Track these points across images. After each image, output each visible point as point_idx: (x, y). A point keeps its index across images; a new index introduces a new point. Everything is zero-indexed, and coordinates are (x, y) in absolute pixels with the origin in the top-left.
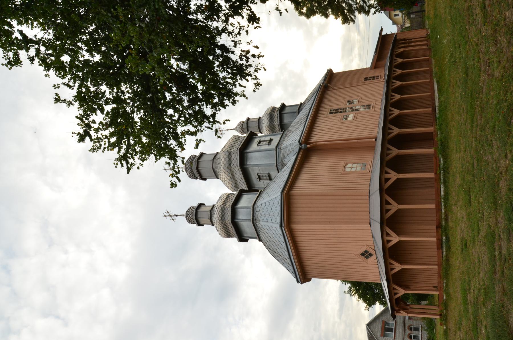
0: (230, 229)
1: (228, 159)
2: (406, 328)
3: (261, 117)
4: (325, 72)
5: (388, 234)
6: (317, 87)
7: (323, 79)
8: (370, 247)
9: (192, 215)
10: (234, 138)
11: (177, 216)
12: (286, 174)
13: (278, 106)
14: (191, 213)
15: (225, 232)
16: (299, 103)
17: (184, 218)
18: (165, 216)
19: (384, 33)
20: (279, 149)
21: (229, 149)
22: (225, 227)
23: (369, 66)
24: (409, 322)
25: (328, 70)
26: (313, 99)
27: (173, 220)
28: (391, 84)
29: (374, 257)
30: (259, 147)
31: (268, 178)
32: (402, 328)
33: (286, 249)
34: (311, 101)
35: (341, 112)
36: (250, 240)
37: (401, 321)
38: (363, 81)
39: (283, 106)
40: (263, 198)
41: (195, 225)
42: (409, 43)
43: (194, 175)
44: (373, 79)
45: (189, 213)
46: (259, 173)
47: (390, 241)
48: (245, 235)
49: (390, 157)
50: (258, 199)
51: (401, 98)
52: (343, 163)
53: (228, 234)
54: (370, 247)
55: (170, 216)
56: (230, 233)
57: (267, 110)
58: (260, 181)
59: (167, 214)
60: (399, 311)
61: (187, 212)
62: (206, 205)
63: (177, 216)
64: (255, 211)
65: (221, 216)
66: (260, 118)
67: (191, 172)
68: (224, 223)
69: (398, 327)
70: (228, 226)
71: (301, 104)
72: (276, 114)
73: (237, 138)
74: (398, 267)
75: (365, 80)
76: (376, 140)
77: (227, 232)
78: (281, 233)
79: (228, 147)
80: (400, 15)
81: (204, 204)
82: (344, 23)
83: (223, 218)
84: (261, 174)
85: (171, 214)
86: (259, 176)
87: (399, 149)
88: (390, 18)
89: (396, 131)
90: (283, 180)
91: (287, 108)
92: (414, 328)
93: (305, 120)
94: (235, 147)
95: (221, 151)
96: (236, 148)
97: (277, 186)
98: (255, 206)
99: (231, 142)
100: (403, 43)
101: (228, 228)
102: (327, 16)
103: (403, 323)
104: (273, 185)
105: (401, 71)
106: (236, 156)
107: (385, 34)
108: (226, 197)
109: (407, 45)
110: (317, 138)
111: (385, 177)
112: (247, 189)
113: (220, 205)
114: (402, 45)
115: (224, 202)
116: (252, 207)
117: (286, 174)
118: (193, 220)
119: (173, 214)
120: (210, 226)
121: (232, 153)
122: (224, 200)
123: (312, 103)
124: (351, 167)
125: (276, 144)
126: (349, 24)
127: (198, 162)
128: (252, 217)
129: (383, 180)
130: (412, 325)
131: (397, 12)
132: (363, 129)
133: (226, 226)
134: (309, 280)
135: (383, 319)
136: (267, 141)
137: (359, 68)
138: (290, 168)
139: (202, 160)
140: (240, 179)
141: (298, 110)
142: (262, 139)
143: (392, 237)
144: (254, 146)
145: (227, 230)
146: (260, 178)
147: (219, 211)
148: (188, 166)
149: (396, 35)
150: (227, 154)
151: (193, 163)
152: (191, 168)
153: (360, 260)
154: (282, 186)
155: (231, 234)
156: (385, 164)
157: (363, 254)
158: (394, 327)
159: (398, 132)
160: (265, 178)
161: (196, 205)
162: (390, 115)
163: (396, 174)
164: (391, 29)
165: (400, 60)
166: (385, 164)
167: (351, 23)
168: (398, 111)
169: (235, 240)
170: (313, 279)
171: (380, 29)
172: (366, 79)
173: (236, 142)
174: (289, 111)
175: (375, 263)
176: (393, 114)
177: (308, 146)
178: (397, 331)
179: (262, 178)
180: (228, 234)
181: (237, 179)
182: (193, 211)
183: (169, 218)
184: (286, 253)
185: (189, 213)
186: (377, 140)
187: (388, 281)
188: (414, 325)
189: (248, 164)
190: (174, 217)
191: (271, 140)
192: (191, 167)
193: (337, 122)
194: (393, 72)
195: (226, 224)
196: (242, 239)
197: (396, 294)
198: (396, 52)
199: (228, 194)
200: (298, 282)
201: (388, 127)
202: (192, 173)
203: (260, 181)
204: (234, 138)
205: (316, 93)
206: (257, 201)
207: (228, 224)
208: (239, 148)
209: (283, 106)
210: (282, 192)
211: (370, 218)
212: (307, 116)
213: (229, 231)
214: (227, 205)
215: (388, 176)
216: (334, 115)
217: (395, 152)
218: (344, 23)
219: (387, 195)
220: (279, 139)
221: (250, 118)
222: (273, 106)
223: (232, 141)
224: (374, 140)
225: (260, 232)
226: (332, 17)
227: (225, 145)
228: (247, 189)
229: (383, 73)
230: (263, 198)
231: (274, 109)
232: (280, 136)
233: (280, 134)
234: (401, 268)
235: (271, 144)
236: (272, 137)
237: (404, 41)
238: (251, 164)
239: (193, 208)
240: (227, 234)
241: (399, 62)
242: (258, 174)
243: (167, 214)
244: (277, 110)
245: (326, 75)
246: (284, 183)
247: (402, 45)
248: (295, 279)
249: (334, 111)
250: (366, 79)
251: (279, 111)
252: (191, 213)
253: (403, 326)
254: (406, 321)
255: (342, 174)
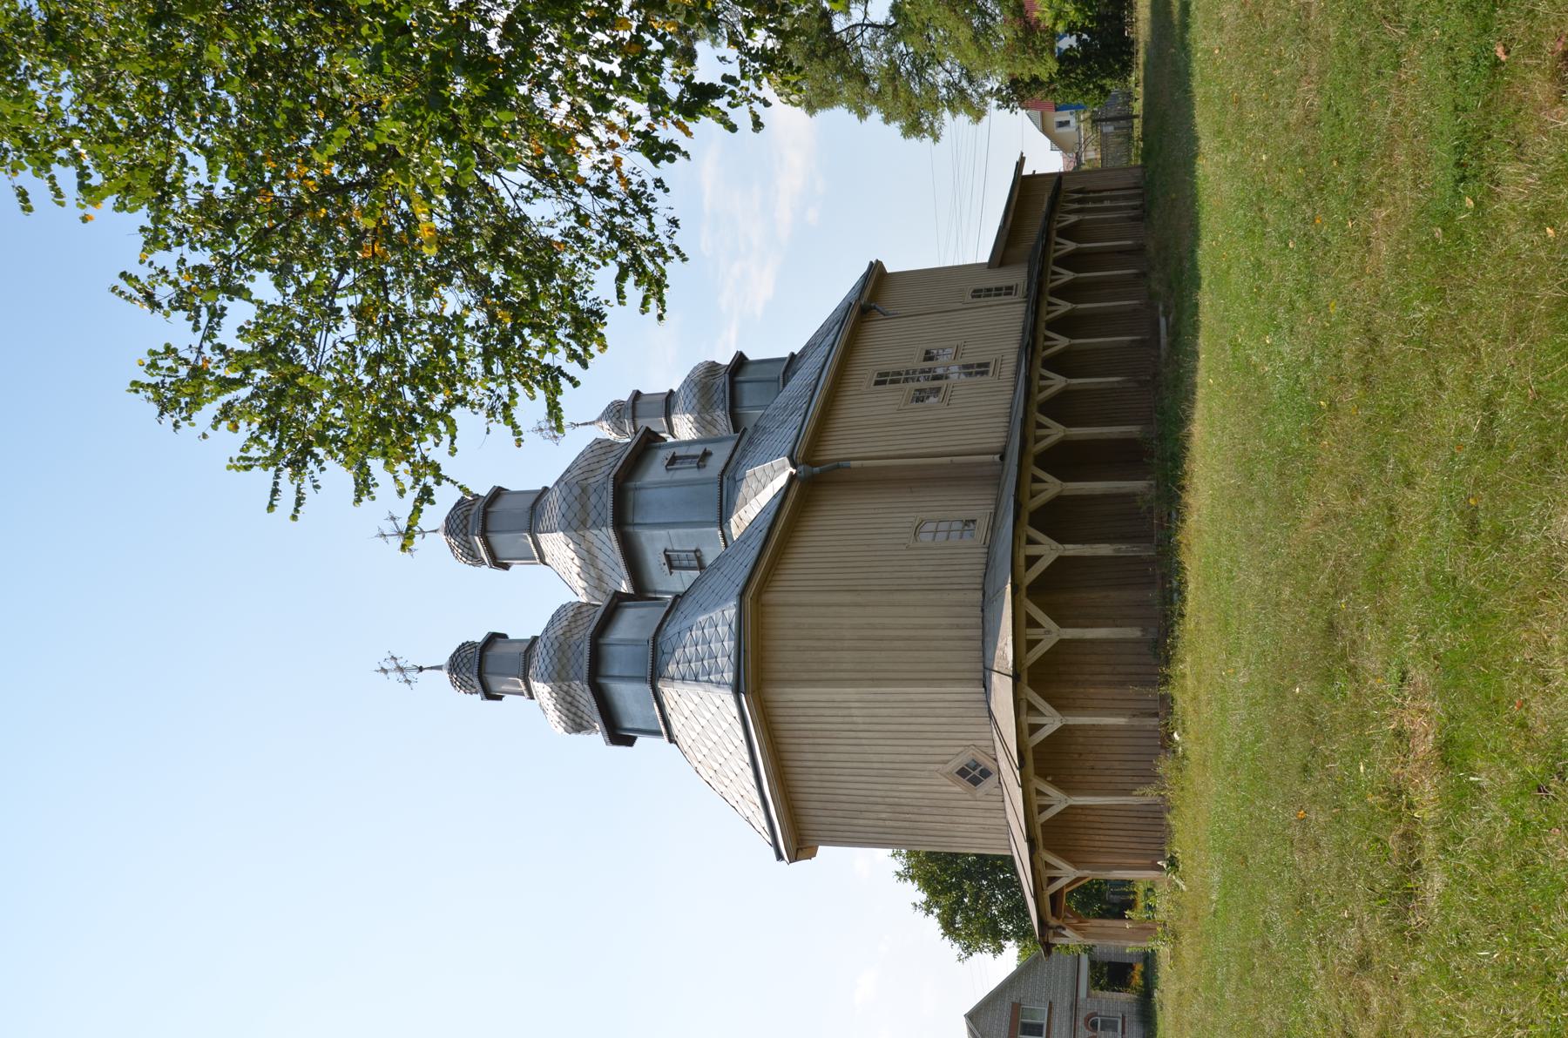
0: (582, 708)
1: (577, 506)
2: (1081, 1023)
3: (675, 390)
4: (863, 269)
5: (1032, 708)
6: (838, 311)
7: (857, 288)
8: (985, 753)
9: (465, 522)
10: (599, 446)
11: (421, 669)
12: (752, 546)
13: (725, 359)
14: (465, 661)
15: (567, 716)
16: (786, 355)
17: (444, 674)
18: (385, 671)
19: (1027, 171)
20: (731, 482)
21: (583, 477)
22: (569, 699)
23: (984, 257)
24: (1088, 1007)
25: (871, 262)
26: (831, 342)
27: (408, 682)
28: (1044, 308)
29: (993, 780)
30: (671, 473)
31: (695, 563)
32: (1068, 1023)
33: (747, 758)
34: (825, 348)
35: (906, 380)
36: (642, 741)
37: (1066, 1004)
38: (968, 298)
39: (740, 360)
40: (683, 616)
41: (478, 696)
42: (1095, 200)
43: (471, 553)
44: (996, 295)
45: (459, 659)
46: (670, 548)
47: (1039, 727)
48: (628, 726)
49: (1044, 499)
50: (668, 619)
51: (1071, 345)
52: (912, 519)
53: (578, 720)
54: (985, 753)
55: (401, 669)
56: (581, 718)
57: (692, 372)
58: (671, 573)
59: (390, 665)
60: (1059, 930)
61: (463, 644)
62: (511, 637)
63: (421, 669)
64: (660, 653)
65: (558, 667)
66: (671, 392)
67: (463, 543)
68: (565, 688)
69: (1056, 1022)
70: (578, 697)
71: (793, 355)
72: (722, 380)
73: (601, 447)
74: (1059, 801)
75: (973, 297)
76: (1002, 458)
77: (575, 714)
78: (735, 712)
79: (580, 471)
80: (1073, 121)
81: (504, 636)
82: (906, 134)
83: (563, 674)
84: (674, 551)
85: (401, 663)
86: (668, 557)
87: (1064, 479)
88: (1045, 130)
89: (1056, 432)
90: (744, 564)
91: (750, 368)
92: (1102, 1021)
93: (807, 399)
94: (600, 471)
95: (557, 483)
96: (603, 475)
97: (726, 579)
98: (660, 639)
99: (587, 457)
100: (1079, 201)
101: (576, 703)
102: (863, 114)
103: (1071, 1010)
104: (715, 578)
105: (1071, 273)
106: (604, 499)
107: (1031, 173)
108: (572, 614)
109: (1090, 205)
110: (843, 446)
111: (1027, 553)
112: (632, 592)
113: (554, 636)
114: (1076, 206)
115: (567, 629)
116: (651, 642)
117: (752, 546)
118: (470, 682)
119: (409, 665)
120: (524, 699)
121: (591, 490)
122: (566, 623)
123: (826, 353)
124: (933, 529)
125: (722, 465)
126: (936, 138)
127: (486, 514)
128: (649, 671)
129: (1022, 561)
130: (1095, 1014)
131: (1065, 116)
132: (889, 742)
133: (573, 697)
134: (812, 854)
135: (1014, 999)
136: (694, 457)
137: (956, 264)
138: (765, 531)
139: (496, 508)
140: (613, 565)
141: (784, 373)
142: (680, 452)
143: (1042, 715)
144: (656, 471)
145: (574, 710)
146: (671, 563)
147: (552, 652)
148: (455, 526)
149: (1059, 177)
150: (576, 491)
151: (471, 518)
152: (464, 531)
153: (958, 789)
154: (741, 579)
155: (585, 723)
156: (1025, 517)
157: (962, 772)
158: (1045, 1022)
159: (1061, 434)
160: (685, 563)
161: (479, 638)
162: (1038, 440)
163: (1055, 544)
164: (1047, 160)
165: (1070, 246)
166: (1025, 517)
167: (928, 140)
168: (1063, 379)
169: (596, 739)
170: (821, 849)
171: (1017, 159)
172: (977, 293)
173: (603, 457)
174: (758, 376)
175: (995, 798)
176: (1051, 386)
177: (816, 469)
178: (1055, 1031)
179: (676, 563)
180: (578, 720)
181: (601, 565)
182: (469, 656)
183: (394, 676)
184: (750, 772)
185: (459, 659)
186: (1007, 460)
187: (1031, 840)
188: (1103, 1014)
189: (637, 520)
190: (411, 675)
191: (706, 454)
192: (465, 527)
193: (897, 407)
194: (1049, 277)
195: (572, 692)
196: (619, 736)
197: (1052, 880)
198: (1059, 222)
199: (578, 605)
200: (780, 857)
201: (1037, 422)
202: (468, 546)
203: (671, 573)
204: (599, 446)
205: (837, 327)
206: (665, 626)
207: (579, 692)
208: (611, 476)
209: (740, 360)
210: (742, 595)
211: (985, 668)
212: (812, 387)
213: (580, 713)
214: (576, 637)
215: (1033, 550)
216: (888, 386)
217: (1053, 487)
218: (906, 134)
219: (1029, 602)
220: (728, 452)
221: (644, 391)
222: (710, 359)
223: (591, 455)
224: (997, 457)
225: (672, 714)
226: (876, 116)
227: (571, 467)
228: (632, 592)
229: (1017, 276)
230: (683, 616)
231: (712, 368)
232: (732, 444)
233: (732, 438)
234: (1066, 805)
235: (705, 466)
236: (710, 447)
237: (1080, 195)
238: (648, 521)
239: (472, 645)
240: (573, 720)
241: (1070, 249)
242: (665, 551)
243: (390, 665)
244: (723, 371)
245: (866, 277)
246: (747, 571)
247: (1076, 206)
248: (772, 851)
249: (889, 378)
250: (977, 293)
251: (730, 374)
252: (465, 661)
253: (1071, 1018)
254: (1080, 1003)
255: (908, 548)
